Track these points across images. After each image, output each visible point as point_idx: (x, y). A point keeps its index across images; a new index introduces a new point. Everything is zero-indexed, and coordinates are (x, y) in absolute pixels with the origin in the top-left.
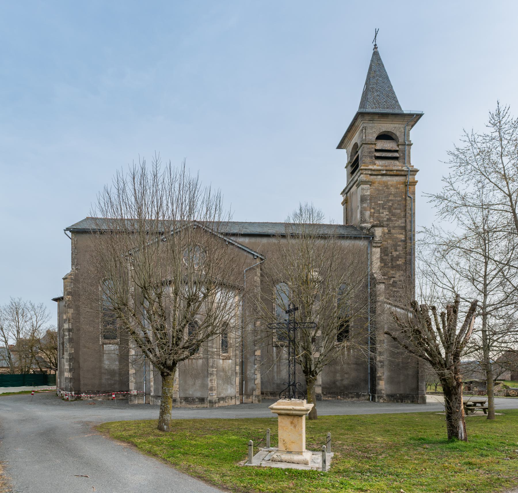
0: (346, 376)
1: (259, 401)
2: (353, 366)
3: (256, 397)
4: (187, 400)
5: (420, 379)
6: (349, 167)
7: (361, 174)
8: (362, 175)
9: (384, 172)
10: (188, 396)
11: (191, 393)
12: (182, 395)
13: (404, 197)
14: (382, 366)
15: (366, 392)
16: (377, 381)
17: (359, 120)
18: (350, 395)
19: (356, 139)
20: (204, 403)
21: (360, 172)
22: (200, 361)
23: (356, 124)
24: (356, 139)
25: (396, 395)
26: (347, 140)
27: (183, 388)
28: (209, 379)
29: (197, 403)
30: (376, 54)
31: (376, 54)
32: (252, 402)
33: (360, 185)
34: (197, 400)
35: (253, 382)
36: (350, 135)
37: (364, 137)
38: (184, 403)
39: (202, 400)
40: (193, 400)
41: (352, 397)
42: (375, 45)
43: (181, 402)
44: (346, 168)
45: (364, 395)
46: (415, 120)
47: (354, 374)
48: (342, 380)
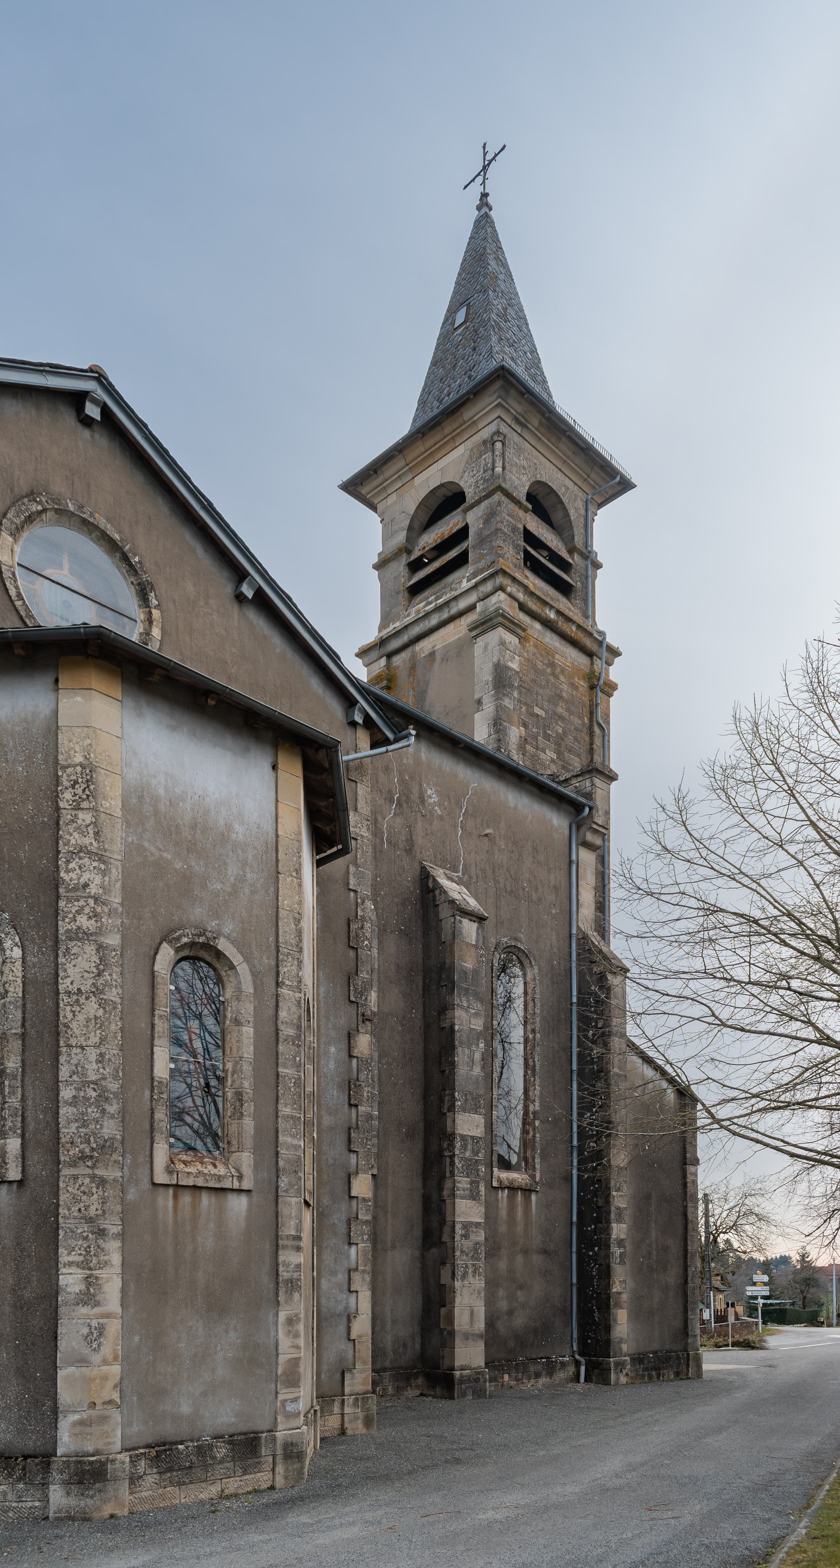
0: (521, 1295)
1: (368, 1422)
2: (537, 1259)
3: (355, 1403)
4: (166, 1456)
5: (689, 1299)
6: (400, 567)
7: (502, 588)
8: (501, 596)
9: (552, 615)
10: (168, 1430)
11: (186, 1409)
12: (142, 1431)
13: (586, 720)
14: (622, 1262)
15: (566, 1352)
16: (613, 1311)
17: (489, 400)
18: (532, 1368)
19: (451, 466)
20: (257, 1467)
21: (500, 580)
22: (239, 1205)
23: (467, 414)
24: (451, 466)
25: (645, 1354)
26: (399, 463)
27: (143, 1384)
28: (282, 1316)
29: (220, 1470)
30: (484, 224)
31: (484, 224)
32: (343, 1432)
33: (494, 627)
34: (221, 1451)
35: (342, 1328)
36: (420, 448)
37: (499, 470)
38: (151, 1479)
39: (246, 1446)
40: (203, 1451)
41: (537, 1375)
42: (485, 195)
43: (134, 1480)
44: (378, 567)
45: (563, 1364)
46: (610, 493)
47: (538, 1289)
48: (510, 1313)
